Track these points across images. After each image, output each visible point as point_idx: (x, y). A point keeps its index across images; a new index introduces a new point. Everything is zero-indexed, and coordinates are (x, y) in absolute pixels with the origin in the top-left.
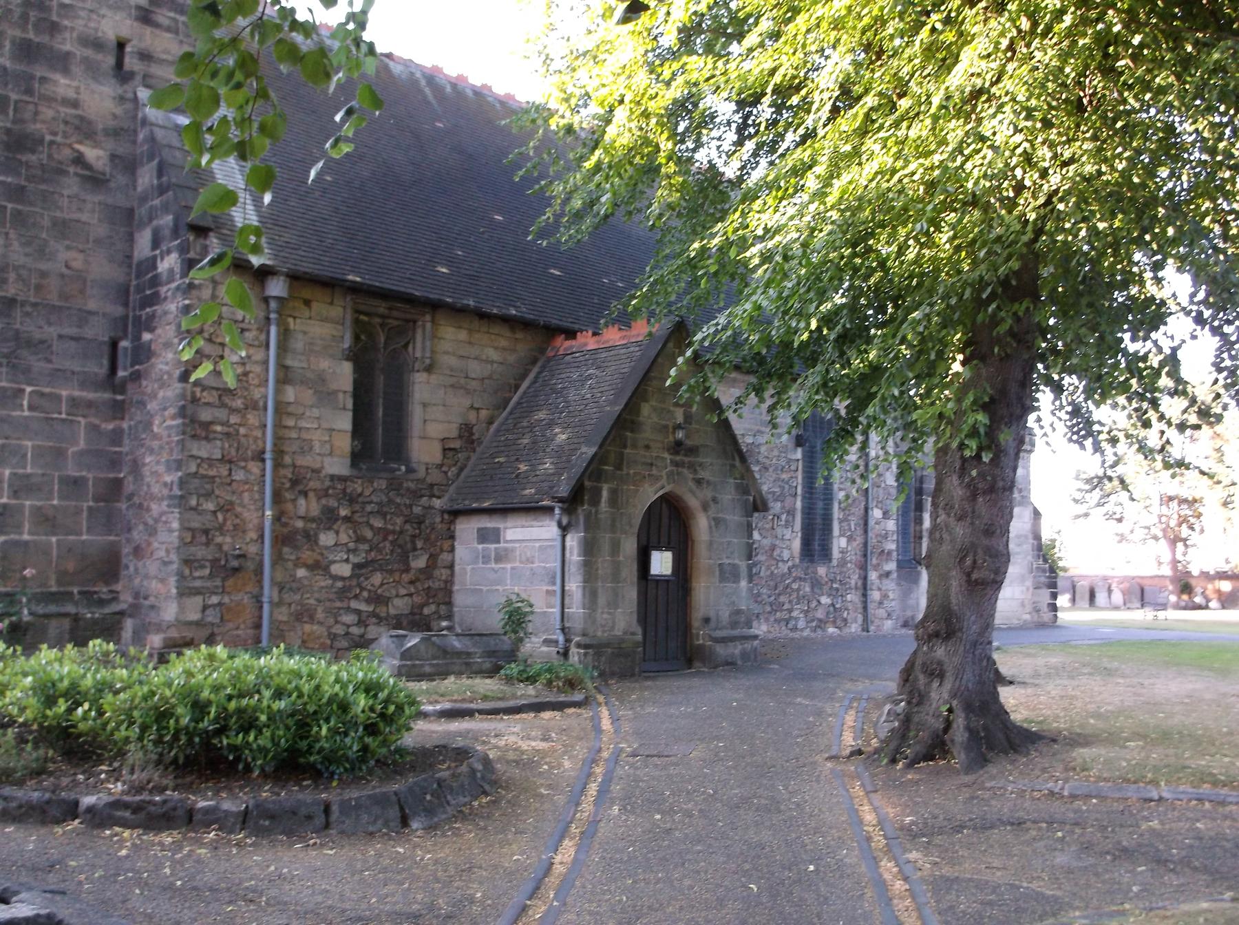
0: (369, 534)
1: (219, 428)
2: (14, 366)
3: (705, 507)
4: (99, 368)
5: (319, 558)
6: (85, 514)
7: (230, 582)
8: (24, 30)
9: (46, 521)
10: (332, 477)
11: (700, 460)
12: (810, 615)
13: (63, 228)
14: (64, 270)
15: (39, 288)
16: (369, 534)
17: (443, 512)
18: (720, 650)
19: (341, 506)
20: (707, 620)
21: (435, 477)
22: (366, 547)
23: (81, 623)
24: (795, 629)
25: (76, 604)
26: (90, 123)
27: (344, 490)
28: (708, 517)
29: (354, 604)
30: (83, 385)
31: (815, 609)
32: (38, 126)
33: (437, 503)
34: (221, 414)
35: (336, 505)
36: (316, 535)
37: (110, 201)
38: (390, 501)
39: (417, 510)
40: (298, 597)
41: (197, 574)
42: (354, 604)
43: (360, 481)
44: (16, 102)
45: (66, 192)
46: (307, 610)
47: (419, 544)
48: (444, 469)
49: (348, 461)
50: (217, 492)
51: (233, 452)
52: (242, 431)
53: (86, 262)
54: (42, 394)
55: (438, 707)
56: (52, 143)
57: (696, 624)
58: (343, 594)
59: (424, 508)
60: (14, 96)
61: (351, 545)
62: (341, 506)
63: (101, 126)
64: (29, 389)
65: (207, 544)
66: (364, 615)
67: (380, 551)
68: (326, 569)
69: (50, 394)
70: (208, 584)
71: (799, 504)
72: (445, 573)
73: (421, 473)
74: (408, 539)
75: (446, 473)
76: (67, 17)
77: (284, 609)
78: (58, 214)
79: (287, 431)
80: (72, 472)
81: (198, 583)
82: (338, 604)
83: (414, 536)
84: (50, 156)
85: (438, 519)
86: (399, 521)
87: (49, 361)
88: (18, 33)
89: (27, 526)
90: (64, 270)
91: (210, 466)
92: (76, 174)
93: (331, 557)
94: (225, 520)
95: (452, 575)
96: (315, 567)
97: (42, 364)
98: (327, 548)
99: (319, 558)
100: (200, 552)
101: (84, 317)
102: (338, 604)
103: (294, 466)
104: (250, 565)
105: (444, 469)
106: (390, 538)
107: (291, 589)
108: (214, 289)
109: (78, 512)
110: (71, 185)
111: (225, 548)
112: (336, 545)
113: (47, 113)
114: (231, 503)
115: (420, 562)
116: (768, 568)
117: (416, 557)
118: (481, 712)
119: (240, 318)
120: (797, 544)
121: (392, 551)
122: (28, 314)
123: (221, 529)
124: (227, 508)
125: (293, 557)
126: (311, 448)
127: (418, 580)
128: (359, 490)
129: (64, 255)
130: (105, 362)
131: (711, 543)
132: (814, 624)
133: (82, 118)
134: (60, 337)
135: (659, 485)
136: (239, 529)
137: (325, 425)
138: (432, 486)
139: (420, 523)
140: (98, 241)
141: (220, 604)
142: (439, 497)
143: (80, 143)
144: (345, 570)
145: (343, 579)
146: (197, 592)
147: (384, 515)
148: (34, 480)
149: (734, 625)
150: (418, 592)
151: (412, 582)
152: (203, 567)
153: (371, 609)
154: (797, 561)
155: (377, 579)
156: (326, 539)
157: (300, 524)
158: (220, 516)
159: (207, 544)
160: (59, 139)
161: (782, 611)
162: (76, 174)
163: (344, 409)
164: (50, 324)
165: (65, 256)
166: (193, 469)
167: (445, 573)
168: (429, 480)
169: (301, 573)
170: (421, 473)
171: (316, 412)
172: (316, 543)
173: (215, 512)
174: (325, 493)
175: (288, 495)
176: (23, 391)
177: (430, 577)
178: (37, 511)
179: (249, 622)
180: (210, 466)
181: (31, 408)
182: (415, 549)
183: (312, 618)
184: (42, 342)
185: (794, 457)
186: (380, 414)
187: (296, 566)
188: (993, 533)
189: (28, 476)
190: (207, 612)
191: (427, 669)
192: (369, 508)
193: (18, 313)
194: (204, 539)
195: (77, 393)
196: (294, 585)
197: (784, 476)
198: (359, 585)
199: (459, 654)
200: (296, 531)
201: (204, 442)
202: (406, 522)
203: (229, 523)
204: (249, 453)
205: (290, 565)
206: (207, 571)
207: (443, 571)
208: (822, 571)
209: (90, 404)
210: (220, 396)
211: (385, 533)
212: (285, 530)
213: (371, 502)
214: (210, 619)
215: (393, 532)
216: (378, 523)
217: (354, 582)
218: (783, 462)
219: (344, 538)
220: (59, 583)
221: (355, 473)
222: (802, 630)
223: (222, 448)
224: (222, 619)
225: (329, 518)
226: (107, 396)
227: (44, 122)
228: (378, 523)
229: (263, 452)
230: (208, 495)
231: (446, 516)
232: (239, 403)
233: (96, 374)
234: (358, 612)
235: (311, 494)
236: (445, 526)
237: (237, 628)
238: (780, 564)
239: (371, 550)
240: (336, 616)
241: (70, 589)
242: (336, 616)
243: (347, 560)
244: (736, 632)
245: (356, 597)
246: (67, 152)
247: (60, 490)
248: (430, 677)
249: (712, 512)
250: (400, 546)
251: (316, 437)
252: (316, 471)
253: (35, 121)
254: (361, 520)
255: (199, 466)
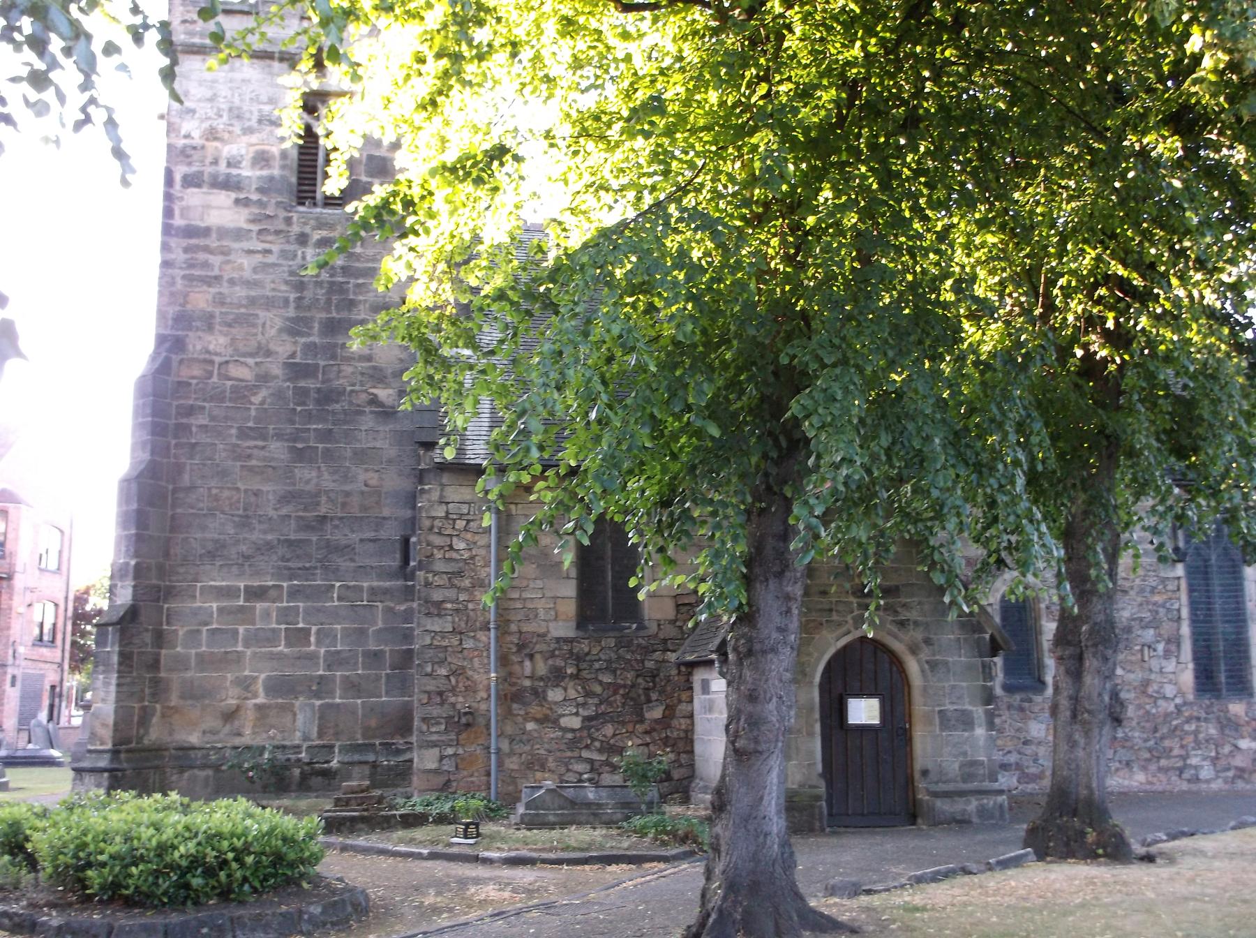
0: (598, 689)
1: (449, 606)
2: (326, 568)
3: (914, 650)
4: (394, 562)
5: (548, 712)
6: (383, 680)
7: (464, 736)
8: (329, 312)
9: (353, 687)
10: (558, 640)
11: (903, 600)
12: (1223, 762)
13: (361, 456)
14: (364, 488)
15: (344, 505)
16: (598, 689)
17: (679, 665)
18: (942, 805)
19: (571, 664)
20: (925, 773)
21: (669, 631)
22: (596, 701)
23: (379, 769)
24: (1196, 779)
25: (377, 753)
26: (381, 370)
27: (571, 651)
28: (919, 661)
29: (585, 754)
30: (380, 577)
31: (1231, 754)
32: (341, 381)
33: (672, 657)
34: (451, 594)
35: (563, 664)
36: (544, 692)
37: (398, 427)
38: (619, 658)
39: (650, 664)
40: (527, 748)
41: (433, 730)
42: (585, 754)
43: (586, 642)
44: (324, 367)
45: (363, 428)
46: (538, 760)
47: (654, 696)
48: (678, 624)
49: (573, 624)
50: (449, 659)
51: (463, 625)
52: (471, 606)
53: (381, 479)
54: (348, 587)
55: (504, 855)
56: (352, 391)
57: (917, 776)
58: (573, 744)
59: (657, 661)
60: (322, 363)
61: (580, 700)
62: (571, 664)
63: (390, 371)
64: (338, 584)
65: (442, 704)
66: (597, 765)
67: (610, 704)
68: (555, 722)
69: (354, 586)
70: (443, 738)
71: (1185, 630)
72: (684, 723)
73: (653, 628)
74: (641, 691)
75: (681, 627)
76: (361, 293)
77: (515, 759)
78: (358, 446)
79: (511, 603)
80: (373, 647)
81: (435, 738)
82: (569, 754)
83: (647, 689)
84: (351, 403)
85: (674, 672)
86: (630, 675)
87: (352, 560)
88: (324, 315)
89: (338, 693)
90: (364, 488)
91: (443, 638)
92: (372, 412)
93: (560, 711)
94: (457, 682)
95: (693, 724)
96: (542, 721)
97: (348, 564)
98: (556, 703)
99: (548, 712)
100: (436, 711)
101: (380, 522)
102: (569, 754)
103: (520, 632)
104: (482, 721)
105: (678, 624)
106: (621, 692)
107: (521, 741)
108: (442, 490)
109: (378, 678)
110: (367, 422)
111: (459, 706)
112: (565, 700)
113: (348, 370)
114: (463, 668)
115: (657, 713)
116: (1139, 707)
117: (652, 708)
118: (544, 861)
119: (466, 511)
120: (1187, 677)
121: (624, 704)
122: (336, 527)
123: (453, 690)
124: (458, 672)
125: (522, 712)
126: (536, 616)
127: (654, 730)
128: (586, 650)
129: (362, 477)
130: (398, 556)
131: (925, 689)
132: (1231, 774)
133: (375, 368)
134: (362, 540)
135: (844, 629)
136: (471, 689)
137: (548, 594)
138: (665, 641)
139: (654, 677)
140: (390, 461)
141: (455, 755)
142: (674, 651)
143: (374, 387)
144: (575, 723)
145: (573, 730)
146: (434, 745)
147: (614, 672)
148: (344, 655)
149: (968, 777)
150: (654, 742)
151: (646, 732)
152: (438, 723)
153: (604, 758)
154: (1191, 697)
155: (609, 730)
156: (555, 695)
157: (527, 683)
158: (453, 680)
159: (442, 704)
160: (357, 388)
161: (1169, 757)
162: (372, 412)
163: (568, 578)
164: (353, 532)
165: (365, 476)
166: (428, 641)
167: (684, 723)
168: (661, 636)
169: (530, 726)
170: (653, 628)
171: (539, 584)
172: (545, 699)
173: (448, 677)
174: (553, 655)
175: (515, 658)
176: (333, 586)
177: (669, 726)
178: (345, 679)
179: (482, 771)
180: (443, 638)
181: (340, 599)
182: (649, 701)
183: (543, 768)
184: (347, 546)
185: (1171, 575)
186: (610, 578)
187: (526, 720)
188: (757, 698)
189: (338, 652)
190: (444, 762)
191: (552, 819)
192: (597, 665)
193: (328, 527)
194: (438, 700)
195: (375, 584)
196: (525, 737)
197: (1157, 598)
198: (590, 736)
199: (589, 805)
200: (524, 689)
201: (436, 619)
202: (638, 676)
203: (461, 685)
204: (478, 624)
205: (520, 719)
206: (443, 727)
207: (682, 721)
208: (1237, 708)
209: (386, 591)
210: (450, 579)
211: (615, 688)
212: (514, 689)
213: (600, 660)
214: (445, 768)
215: (624, 686)
216: (607, 679)
217: (585, 733)
218: (1152, 582)
219: (572, 694)
220: (364, 736)
221: (581, 634)
222: (1208, 781)
223: (453, 622)
224: (457, 767)
225: (557, 677)
226: (400, 583)
227: (345, 377)
228: (607, 679)
229: (489, 623)
230: (441, 662)
231: (683, 669)
232: (467, 583)
233: (390, 566)
234: (591, 761)
235: (538, 657)
236: (683, 678)
237: (472, 776)
238: (1160, 702)
239: (601, 703)
240: (566, 765)
241: (372, 741)
242: (566, 765)
243: (577, 714)
244: (974, 785)
245: (587, 747)
246: (364, 396)
247: (363, 663)
248: (551, 826)
249: (925, 654)
250: (632, 699)
251: (540, 605)
252: (543, 635)
253: (338, 378)
254: (588, 677)
255: (433, 638)
